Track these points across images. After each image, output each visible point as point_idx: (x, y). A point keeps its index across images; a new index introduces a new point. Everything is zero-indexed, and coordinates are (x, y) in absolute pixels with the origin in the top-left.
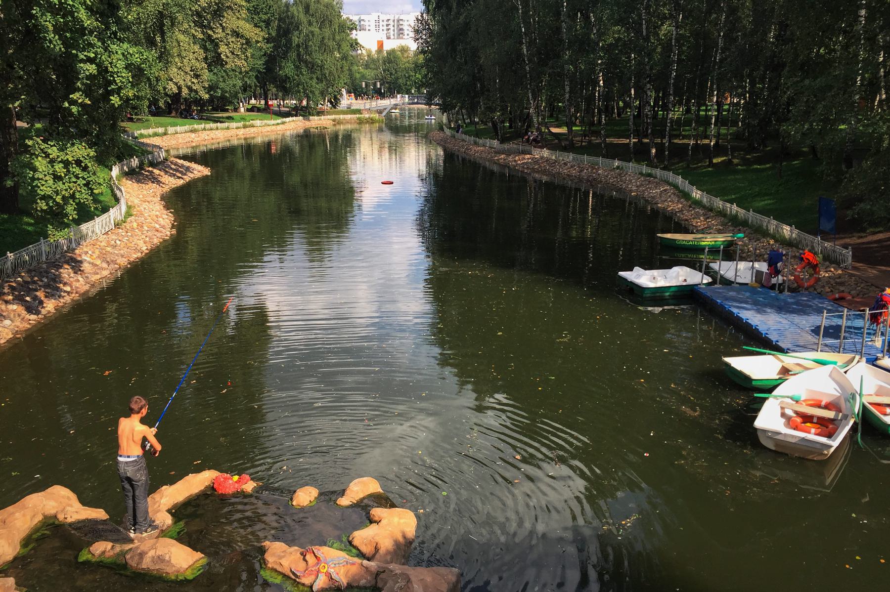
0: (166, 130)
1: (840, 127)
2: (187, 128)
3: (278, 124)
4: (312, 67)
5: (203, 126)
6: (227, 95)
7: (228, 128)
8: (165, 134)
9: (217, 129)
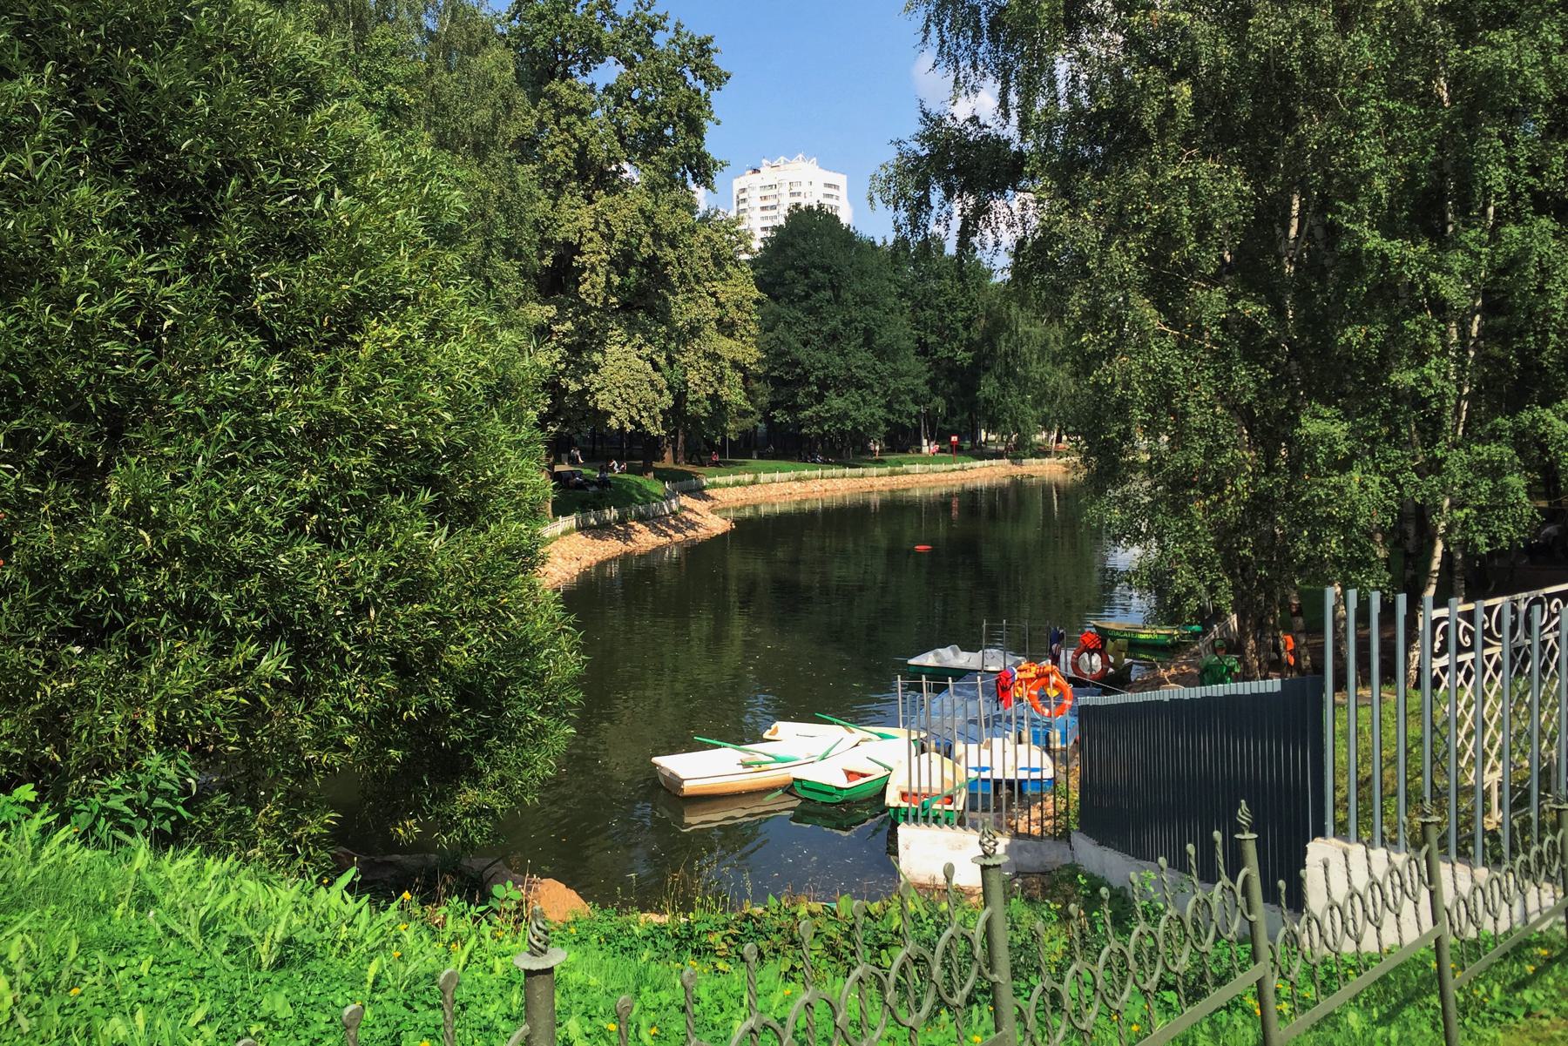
0: (756, 477)
1: (1474, 335)
2: (793, 474)
3: (954, 470)
4: (1024, 383)
5: (819, 472)
6: (861, 428)
7: (863, 476)
8: (753, 483)
9: (844, 476)
